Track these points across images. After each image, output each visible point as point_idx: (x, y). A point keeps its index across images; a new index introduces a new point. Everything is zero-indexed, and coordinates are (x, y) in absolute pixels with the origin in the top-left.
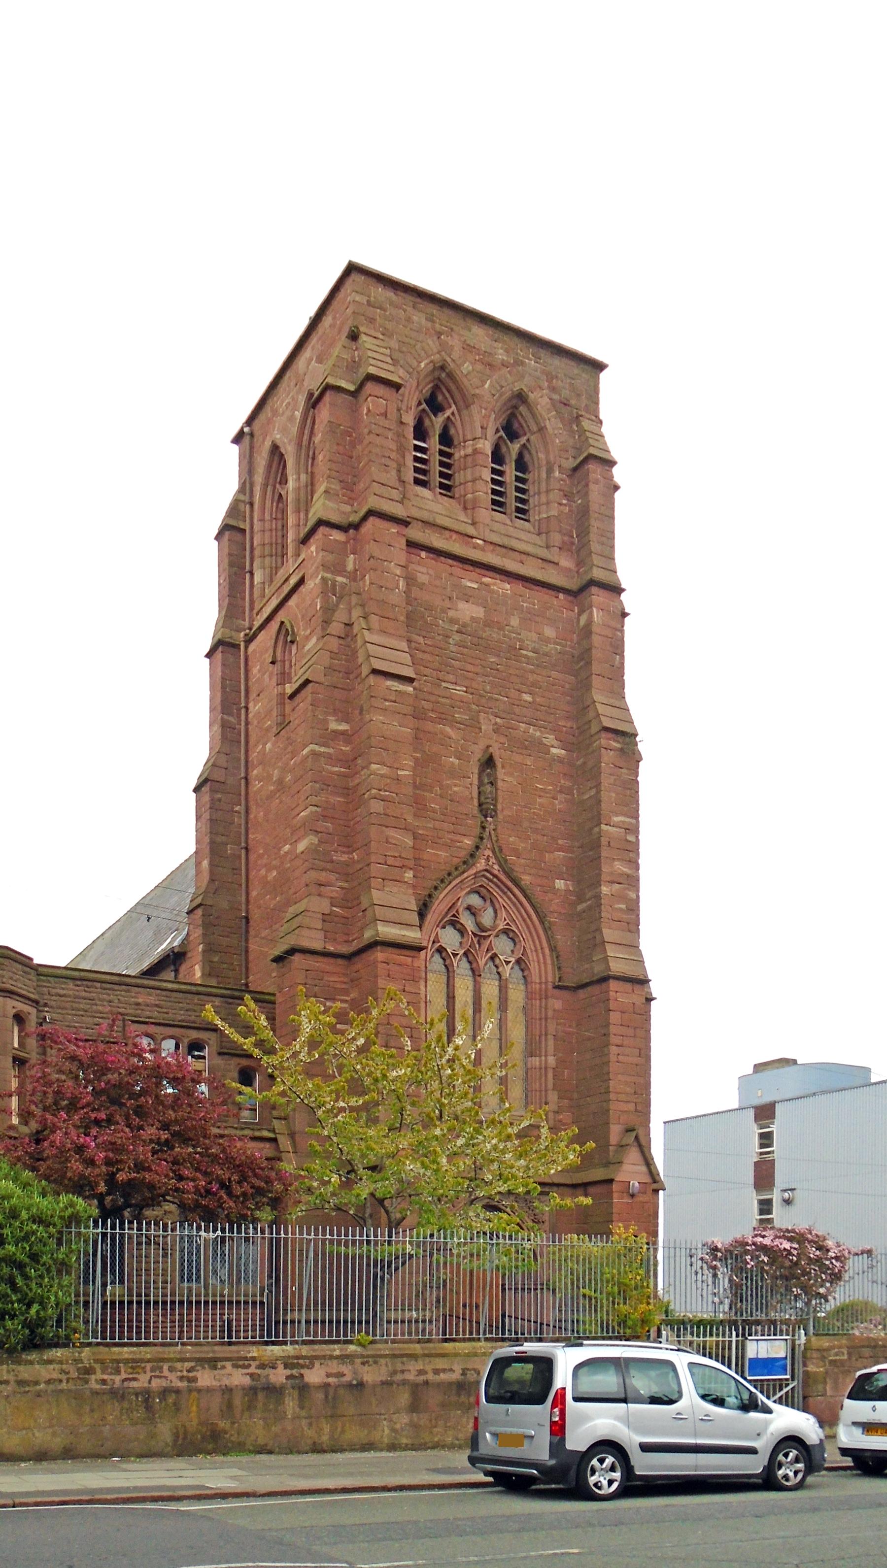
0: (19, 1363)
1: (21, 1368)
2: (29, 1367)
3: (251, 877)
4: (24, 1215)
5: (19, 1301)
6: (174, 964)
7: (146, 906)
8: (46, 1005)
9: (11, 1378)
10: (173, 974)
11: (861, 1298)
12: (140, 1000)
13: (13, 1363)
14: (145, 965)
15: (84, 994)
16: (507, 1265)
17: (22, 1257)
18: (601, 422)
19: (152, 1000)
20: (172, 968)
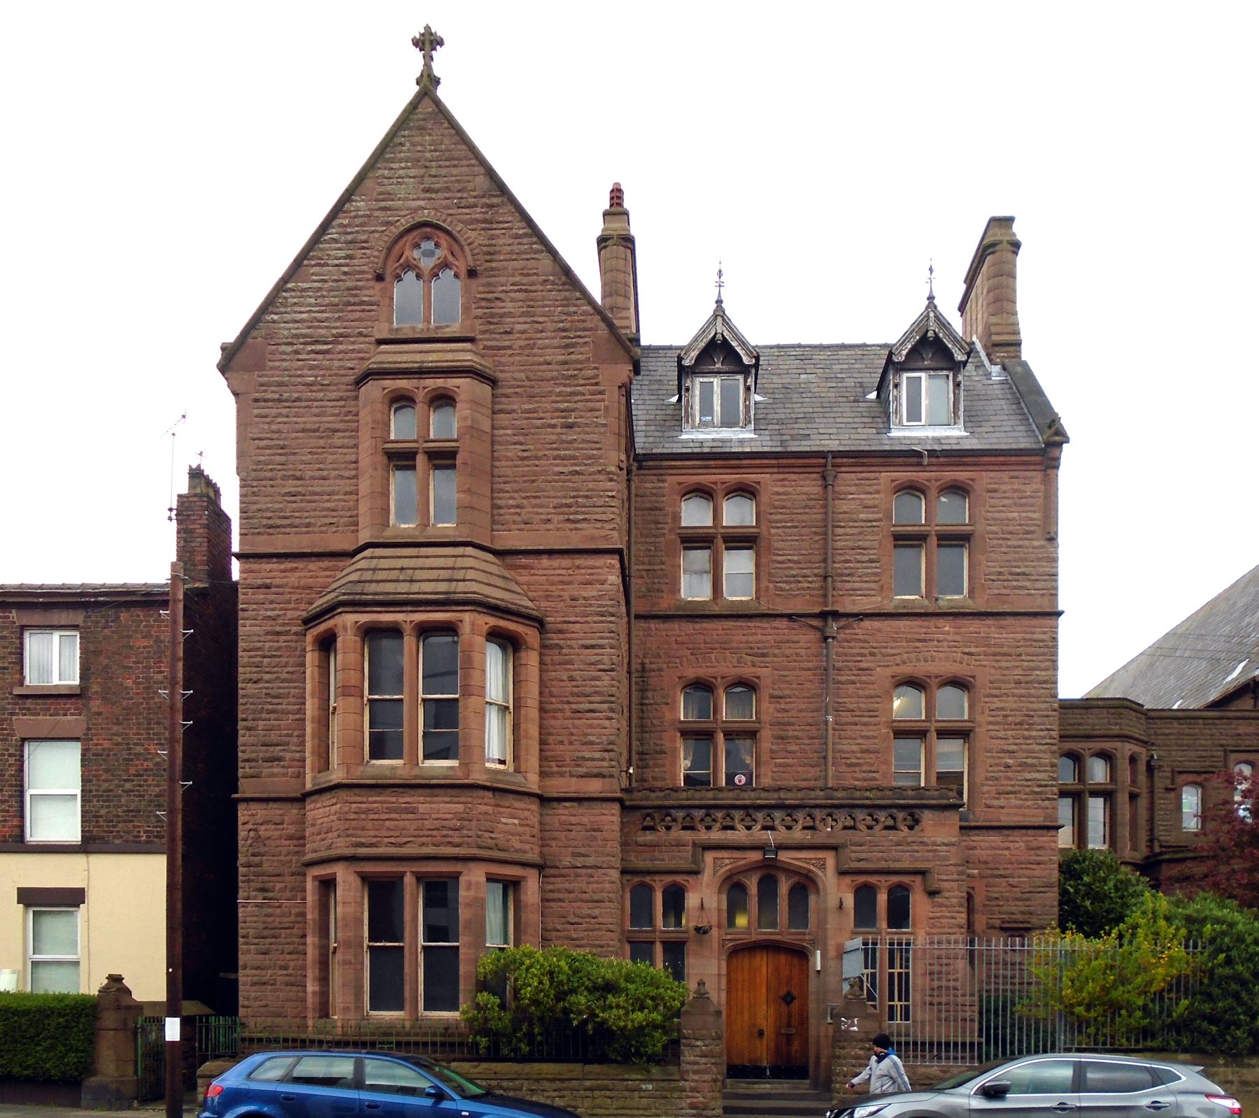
0: (1242, 1065)
1: (1245, 1071)
2: (1252, 1070)
3: (940, 622)
4: (1249, 939)
5: (1245, 1013)
6: (1254, 692)
7: (1200, 637)
8: (1153, 744)
9: (1235, 1078)
10: (1252, 702)
11: (746, 960)
12: (1240, 731)
13: (1238, 1066)
14: (1213, 695)
15: (1187, 731)
16: (1182, 994)
17: (1247, 975)
18: (626, 214)
19: (1251, 730)
20: (1251, 695)
